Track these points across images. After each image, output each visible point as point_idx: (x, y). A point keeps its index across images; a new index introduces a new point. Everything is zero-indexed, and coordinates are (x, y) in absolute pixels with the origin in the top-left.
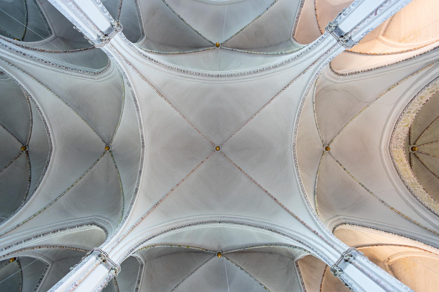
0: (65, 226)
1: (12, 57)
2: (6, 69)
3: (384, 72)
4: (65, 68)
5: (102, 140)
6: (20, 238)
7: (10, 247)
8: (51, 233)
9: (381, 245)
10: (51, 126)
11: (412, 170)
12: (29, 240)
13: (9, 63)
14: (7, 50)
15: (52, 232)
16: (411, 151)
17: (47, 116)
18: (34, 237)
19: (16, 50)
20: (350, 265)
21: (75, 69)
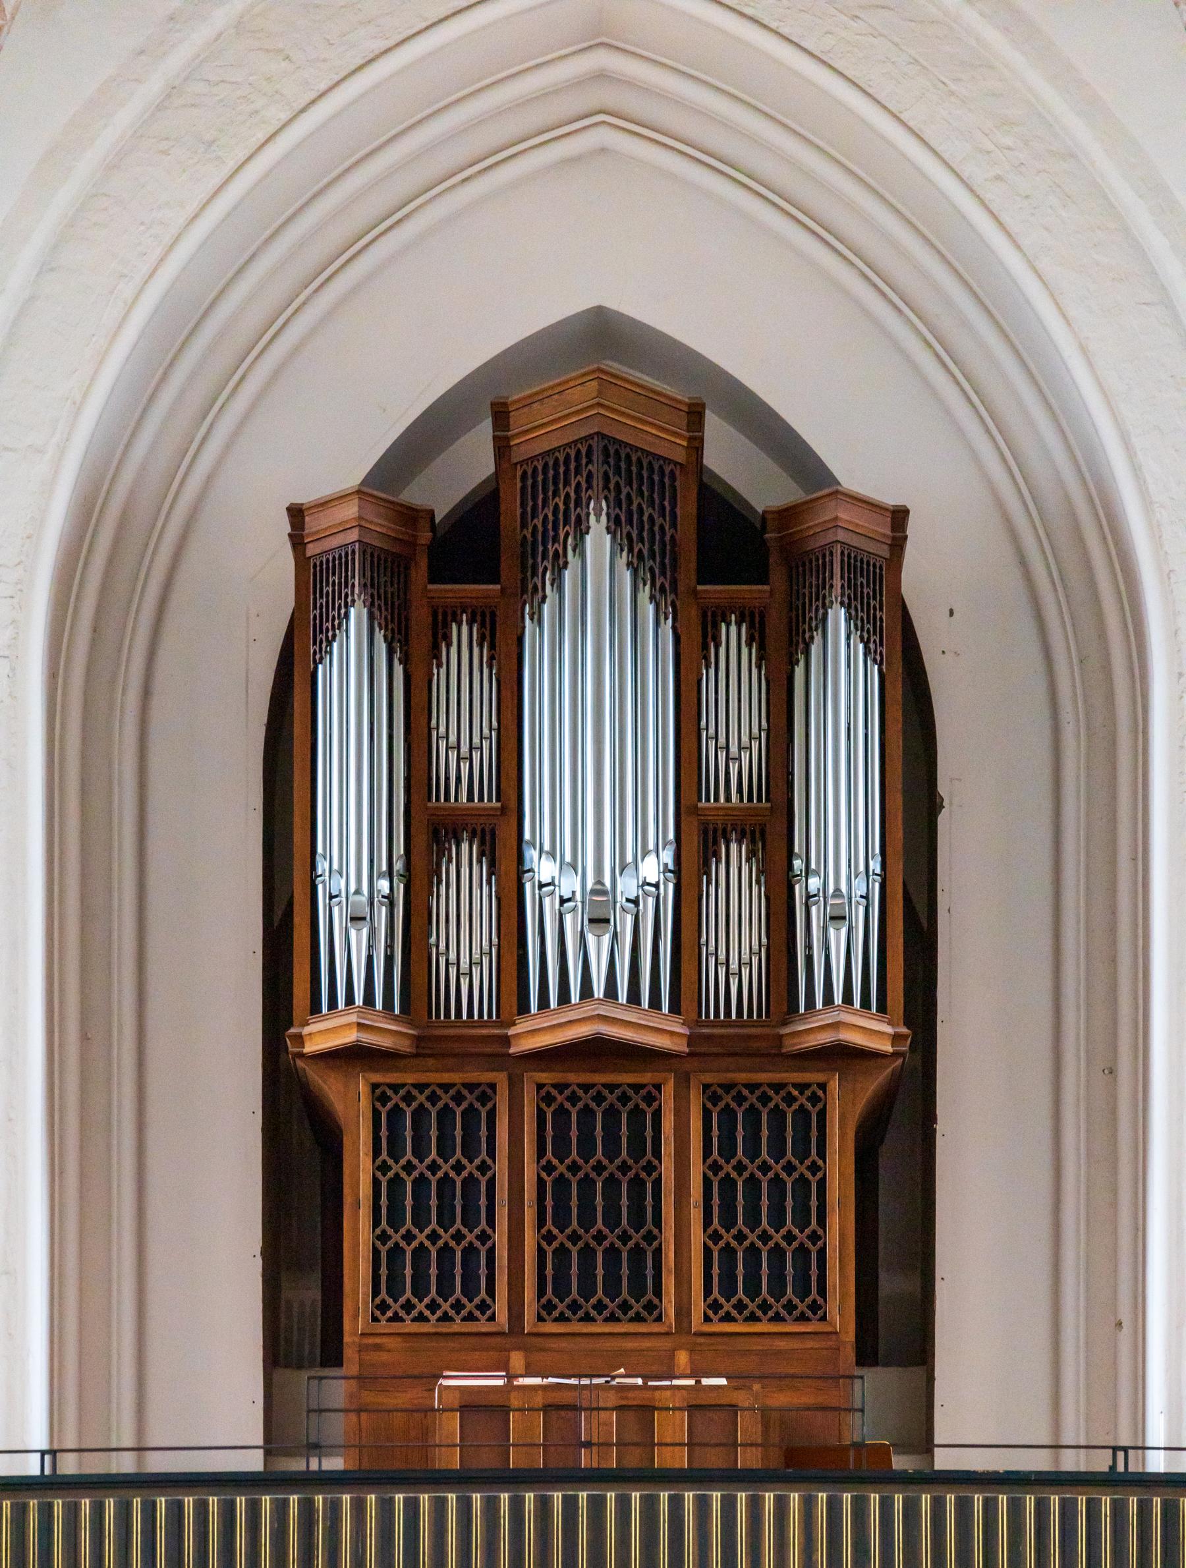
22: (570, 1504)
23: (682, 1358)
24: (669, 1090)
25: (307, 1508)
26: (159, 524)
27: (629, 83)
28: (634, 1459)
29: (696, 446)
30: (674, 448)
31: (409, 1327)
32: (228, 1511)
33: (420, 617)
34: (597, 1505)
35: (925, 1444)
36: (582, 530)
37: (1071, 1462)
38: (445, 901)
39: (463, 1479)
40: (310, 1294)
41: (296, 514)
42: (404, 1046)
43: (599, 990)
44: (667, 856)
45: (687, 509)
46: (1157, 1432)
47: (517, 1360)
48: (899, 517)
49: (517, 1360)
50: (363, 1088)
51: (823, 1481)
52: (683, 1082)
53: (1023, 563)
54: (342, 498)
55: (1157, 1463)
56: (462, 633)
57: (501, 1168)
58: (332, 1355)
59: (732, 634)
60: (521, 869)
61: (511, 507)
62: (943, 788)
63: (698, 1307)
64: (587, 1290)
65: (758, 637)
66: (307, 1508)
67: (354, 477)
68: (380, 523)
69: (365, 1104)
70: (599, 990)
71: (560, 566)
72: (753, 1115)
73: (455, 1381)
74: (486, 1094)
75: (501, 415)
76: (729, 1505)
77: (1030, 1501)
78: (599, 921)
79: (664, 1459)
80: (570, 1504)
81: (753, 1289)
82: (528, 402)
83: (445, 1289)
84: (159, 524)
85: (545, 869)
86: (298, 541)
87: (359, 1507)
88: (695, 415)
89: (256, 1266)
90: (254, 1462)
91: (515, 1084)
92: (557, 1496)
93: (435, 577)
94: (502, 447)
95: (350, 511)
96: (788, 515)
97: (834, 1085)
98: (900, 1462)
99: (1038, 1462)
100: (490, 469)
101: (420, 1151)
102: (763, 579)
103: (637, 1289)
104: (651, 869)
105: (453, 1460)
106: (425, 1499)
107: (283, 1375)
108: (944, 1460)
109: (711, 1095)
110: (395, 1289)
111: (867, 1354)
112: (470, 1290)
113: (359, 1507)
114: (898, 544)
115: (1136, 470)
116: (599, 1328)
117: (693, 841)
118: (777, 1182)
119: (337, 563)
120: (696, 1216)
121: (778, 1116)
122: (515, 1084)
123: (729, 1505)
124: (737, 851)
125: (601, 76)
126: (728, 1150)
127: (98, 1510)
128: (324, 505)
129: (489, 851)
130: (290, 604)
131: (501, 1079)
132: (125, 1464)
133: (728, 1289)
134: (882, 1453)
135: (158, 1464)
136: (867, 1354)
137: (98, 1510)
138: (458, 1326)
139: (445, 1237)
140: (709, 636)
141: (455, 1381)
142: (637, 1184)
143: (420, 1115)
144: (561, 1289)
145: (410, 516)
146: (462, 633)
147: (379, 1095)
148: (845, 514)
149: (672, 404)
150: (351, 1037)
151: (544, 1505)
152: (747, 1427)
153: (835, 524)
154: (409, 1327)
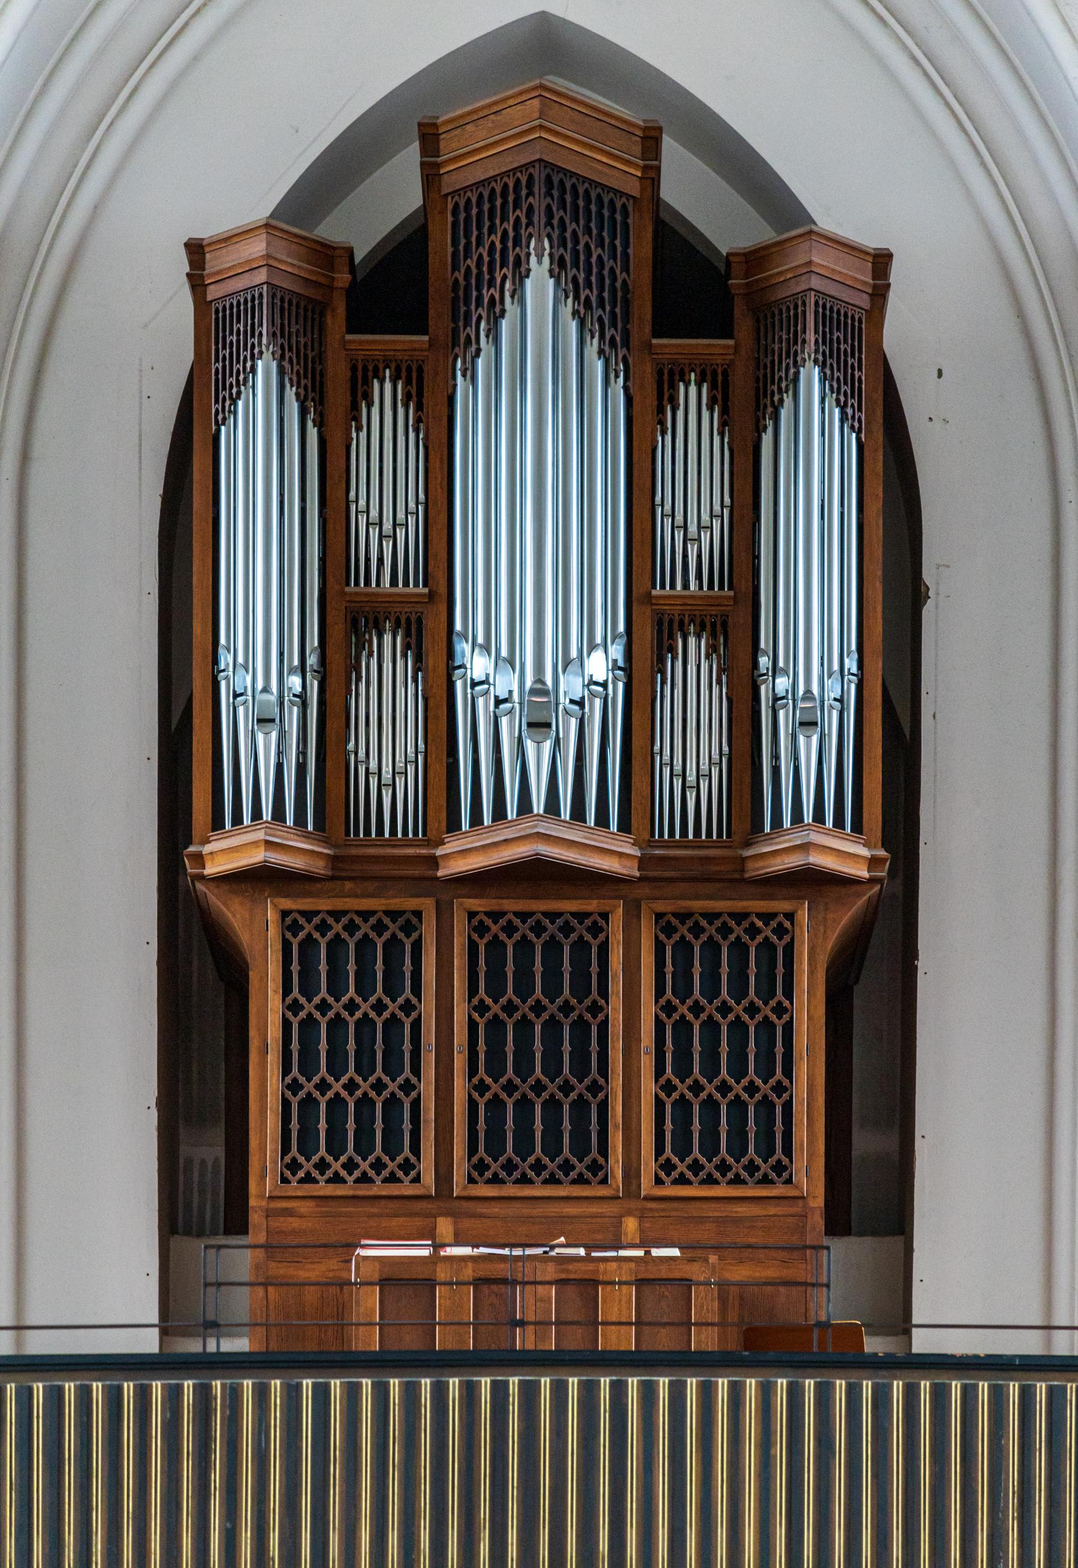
22: (499, 1391)
23: (631, 1225)
28: (575, 1341)
29: (652, 177)
31: (322, 1188)
33: (337, 371)
34: (529, 1392)
36: (521, 274)
41: (196, 250)
42: (319, 867)
43: (538, 805)
44: (617, 651)
45: (642, 249)
47: (445, 1227)
48: (881, 261)
50: (271, 915)
54: (246, 233)
60: (451, 665)
62: (928, 575)
63: (648, 1166)
66: (204, 1394)
67: (263, 210)
68: (290, 261)
69: (273, 933)
70: (538, 805)
71: (496, 316)
74: (411, 923)
76: (352, 1394)
78: (539, 726)
80: (499, 1391)
81: (710, 1148)
83: (364, 1147)
85: (479, 666)
86: (197, 282)
87: (262, 1394)
89: (152, 1118)
90: (148, 1343)
91: (443, 912)
94: (431, 175)
95: (257, 247)
97: (803, 915)
98: (873, 1345)
99: (1029, 1345)
103: (581, 1148)
104: (598, 666)
105: (371, 1341)
106: (97, 1387)
107: (180, 1243)
108: (922, 1342)
112: (391, 1147)
113: (262, 1394)
114: (880, 293)
117: (646, 634)
119: (246, 305)
120: (647, 1063)
121: (739, 949)
122: (443, 912)
123: (677, 1393)
124: (695, 646)
128: (228, 240)
131: (427, 905)
135: (38, 1345)
138: (378, 1188)
142: (581, 1027)
143: (336, 946)
147: (289, 924)
148: (822, 258)
149: (624, 127)
151: (470, 1392)
154: (322, 1188)
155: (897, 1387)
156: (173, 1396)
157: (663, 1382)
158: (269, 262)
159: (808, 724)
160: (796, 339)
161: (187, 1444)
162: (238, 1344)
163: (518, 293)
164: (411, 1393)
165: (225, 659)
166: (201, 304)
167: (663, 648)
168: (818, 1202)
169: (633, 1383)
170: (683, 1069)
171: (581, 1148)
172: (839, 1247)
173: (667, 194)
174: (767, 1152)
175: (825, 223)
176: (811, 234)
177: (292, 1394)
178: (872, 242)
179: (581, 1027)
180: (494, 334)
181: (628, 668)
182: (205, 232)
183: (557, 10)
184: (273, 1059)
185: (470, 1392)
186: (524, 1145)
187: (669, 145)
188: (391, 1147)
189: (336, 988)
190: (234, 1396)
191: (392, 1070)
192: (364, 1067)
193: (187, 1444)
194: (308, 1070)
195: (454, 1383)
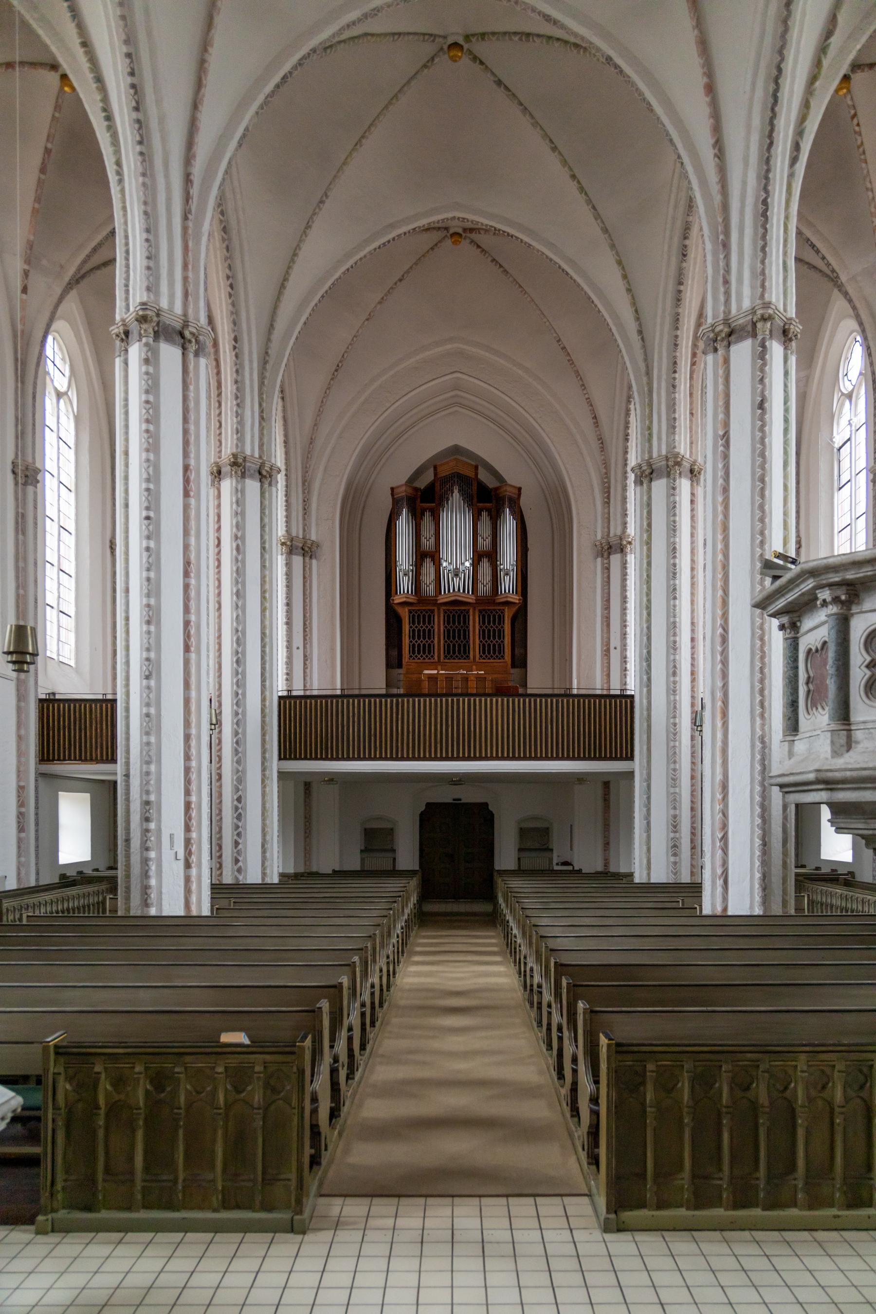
0: (679, 224)
1: (251, 361)
2: (276, 381)
3: (182, 1047)
4: (240, 765)
5: (426, 71)
6: (666, 337)
7: (675, 363)
8: (684, 265)
9: (704, 45)
10: (392, 226)
11: (149, 495)
12: (678, 319)
13: (266, 362)
14: (243, 376)
15: (683, 261)
16: (450, 41)
17: (367, 242)
18: (678, 306)
19: (235, 375)
20: (259, 484)
21: (237, 861)
22: (453, 700)
23: (474, 667)
24: (471, 612)
25: (397, 702)
26: (840, 786)
27: (462, 397)
28: (464, 691)
29: (477, 474)
30: (471, 474)
31: (416, 660)
32: (301, 703)
33: (419, 511)
34: (458, 701)
35: (525, 685)
36: (452, 493)
37: (556, 692)
38: (424, 570)
39: (430, 695)
40: (395, 653)
41: (392, 489)
42: (415, 601)
43: (456, 590)
44: (471, 561)
45: (475, 488)
46: (575, 684)
47: (439, 667)
48: (520, 489)
49: (439, 667)
50: (407, 610)
51: (505, 696)
52: (474, 609)
53: (545, 496)
54: (402, 486)
55: (575, 692)
56: (427, 514)
57: (436, 627)
58: (400, 666)
59: (484, 514)
60: (440, 564)
61: (437, 488)
62: (529, 546)
63: (478, 656)
64: (454, 653)
65: (490, 515)
66: (397, 702)
67: (404, 481)
68: (410, 491)
69: (407, 614)
70: (456, 590)
71: (448, 500)
72: (489, 616)
73: (426, 672)
74: (433, 611)
75: (435, 468)
76: (425, 701)
77: (549, 700)
78: (457, 575)
79: (455, 691)
80: (453, 700)
81: (489, 653)
82: (441, 465)
83: (424, 653)
84: (840, 786)
85: (445, 564)
86: (392, 495)
87: (408, 701)
88: (476, 468)
89: (384, 647)
90: (384, 692)
91: (439, 609)
92: (455, 699)
93: (421, 502)
94: (436, 474)
95: (404, 488)
96: (497, 489)
97: (506, 610)
98: (521, 691)
99: (549, 692)
100: (432, 478)
101: (419, 624)
102: (490, 502)
103: (465, 652)
104: (467, 564)
105: (426, 691)
106: (455, 699)
107: (390, 670)
108: (529, 691)
109: (480, 611)
110: (414, 653)
111: (513, 666)
112: (429, 653)
113: (408, 701)
114: (519, 495)
115: (571, 481)
116: (457, 661)
117: (476, 558)
118: (494, 630)
119: (402, 499)
120: (477, 637)
121: (494, 616)
122: (439, 609)
123: (425, 701)
124: (485, 560)
125: (456, 396)
126: (484, 623)
127: (354, 702)
128: (398, 487)
129: (433, 560)
130: (391, 507)
131: (435, 608)
132: (356, 692)
133: (484, 653)
134: (517, 688)
135: (364, 692)
136: (513, 666)
137: (354, 702)
138: (427, 660)
139: (424, 642)
140: (480, 514)
141: (426, 672)
142: (465, 631)
143: (419, 616)
144: (449, 653)
145: (416, 489)
146: (427, 514)
147: (410, 612)
148: (509, 489)
149: (472, 465)
150: (404, 600)
151: (447, 701)
152: (488, 684)
153: (506, 491)
154: (416, 660)
155: (527, 700)
156: (392, 702)
157: (483, 699)
158: (406, 491)
159: (507, 574)
160: (504, 504)
161: (394, 711)
162: (401, 691)
163: (452, 496)
164: (436, 701)
165: (398, 564)
166: (393, 499)
167: (479, 560)
168: (509, 662)
169: (477, 699)
170: (484, 638)
171: (465, 652)
172: (513, 671)
173: (479, 477)
174: (500, 653)
175: (509, 482)
176: (507, 485)
177: (414, 702)
178: (518, 486)
179: (465, 631)
180: (447, 503)
181: (473, 564)
182: (394, 486)
183: (464, 443)
184: (506, 633)
185: (447, 701)
186: (454, 653)
187: (480, 468)
188: (429, 653)
189: (419, 624)
190: (403, 702)
191: (429, 638)
192: (424, 638)
193: (394, 711)
194: (414, 639)
195: (444, 699)
